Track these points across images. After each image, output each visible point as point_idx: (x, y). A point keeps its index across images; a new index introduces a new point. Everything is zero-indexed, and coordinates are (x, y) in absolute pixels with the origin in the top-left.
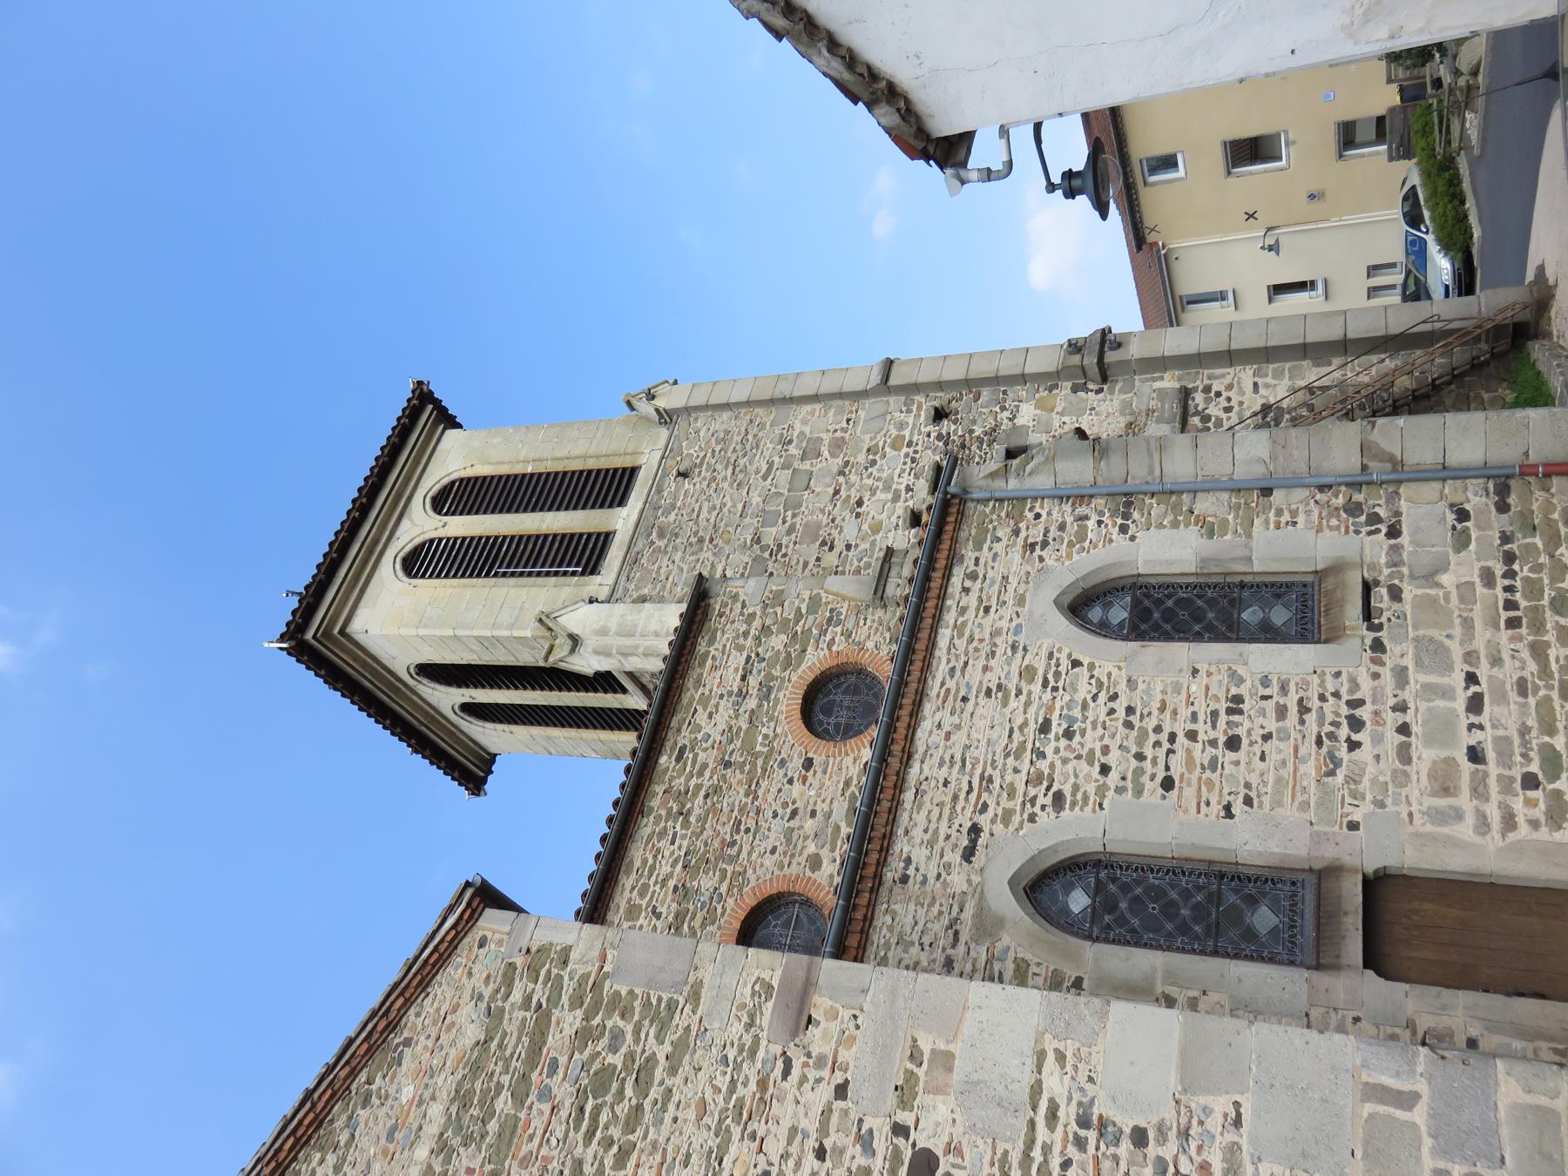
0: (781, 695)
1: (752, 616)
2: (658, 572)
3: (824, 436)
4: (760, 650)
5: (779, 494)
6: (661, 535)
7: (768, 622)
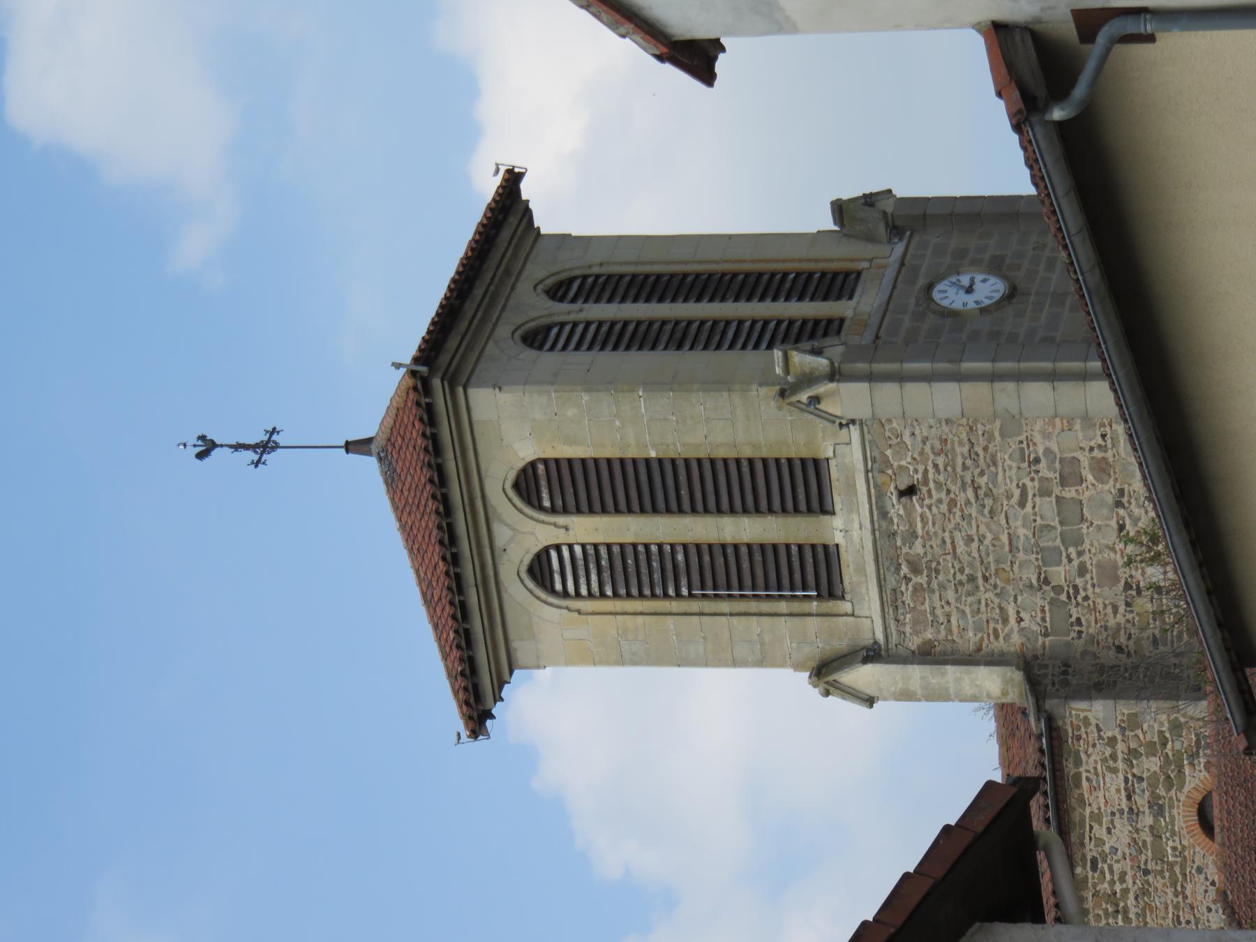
0: (1175, 811)
1: (1112, 741)
2: (933, 613)
3: (1078, 455)
4: (1135, 771)
5: (1049, 528)
6: (916, 569)
7: (1133, 745)
